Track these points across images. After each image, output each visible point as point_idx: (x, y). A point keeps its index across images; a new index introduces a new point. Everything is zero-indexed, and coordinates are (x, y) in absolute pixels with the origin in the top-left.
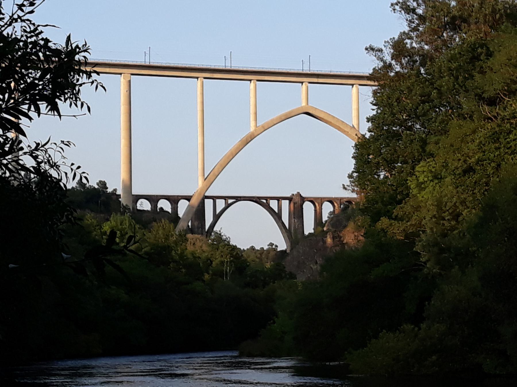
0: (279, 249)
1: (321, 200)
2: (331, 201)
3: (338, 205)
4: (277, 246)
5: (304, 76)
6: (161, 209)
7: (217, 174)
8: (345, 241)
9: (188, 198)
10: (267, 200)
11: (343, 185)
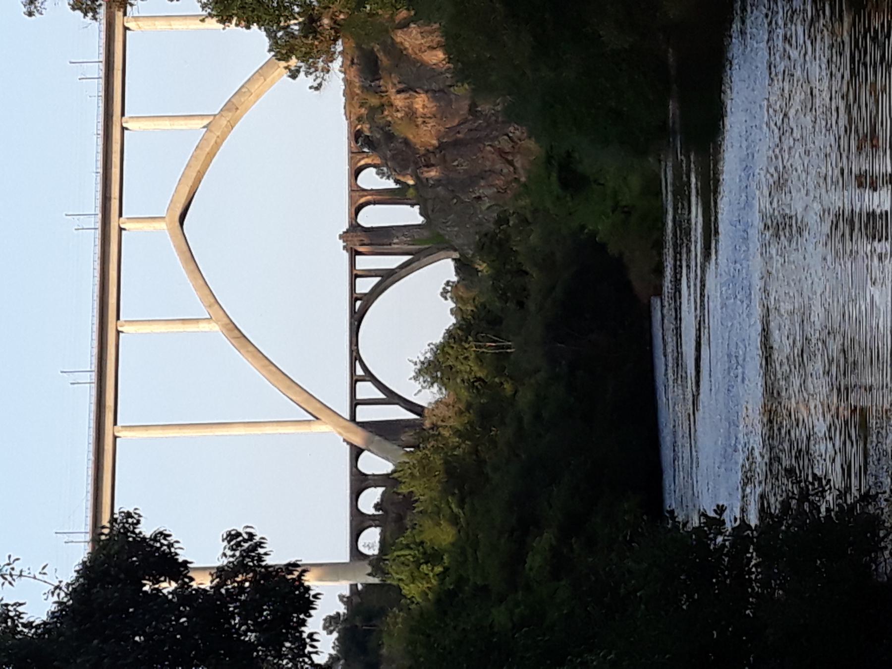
0: (455, 279)
1: (353, 190)
2: (356, 172)
3: (363, 158)
4: (448, 283)
5: (107, 227)
6: (377, 507)
7: (306, 395)
8: (435, 142)
9: (356, 453)
10: (357, 299)
11: (311, 88)
